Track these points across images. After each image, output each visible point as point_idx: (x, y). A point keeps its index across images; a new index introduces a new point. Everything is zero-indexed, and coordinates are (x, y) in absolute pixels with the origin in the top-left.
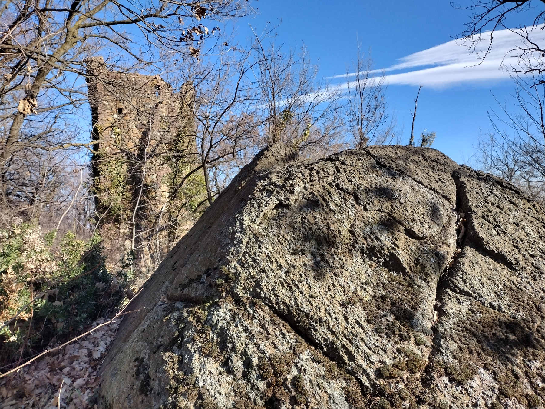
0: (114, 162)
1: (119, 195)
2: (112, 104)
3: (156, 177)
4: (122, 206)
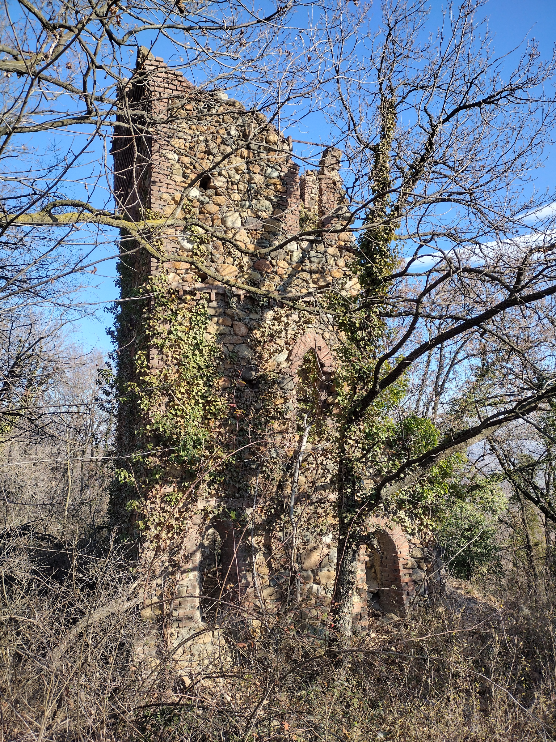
0: (188, 314)
1: (197, 403)
2: (186, 160)
3: (288, 359)
4: (203, 434)
